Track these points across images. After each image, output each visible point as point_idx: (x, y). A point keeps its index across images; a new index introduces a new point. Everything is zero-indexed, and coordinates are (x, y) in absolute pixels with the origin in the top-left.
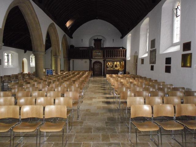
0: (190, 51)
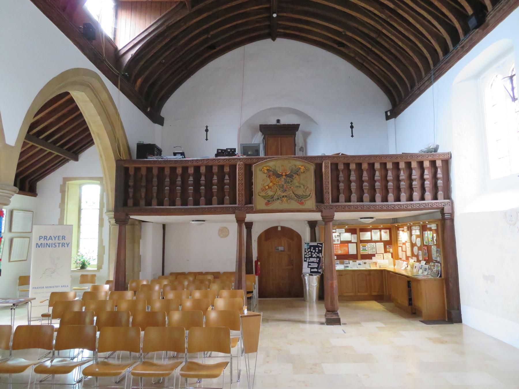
0: (245, 272)
